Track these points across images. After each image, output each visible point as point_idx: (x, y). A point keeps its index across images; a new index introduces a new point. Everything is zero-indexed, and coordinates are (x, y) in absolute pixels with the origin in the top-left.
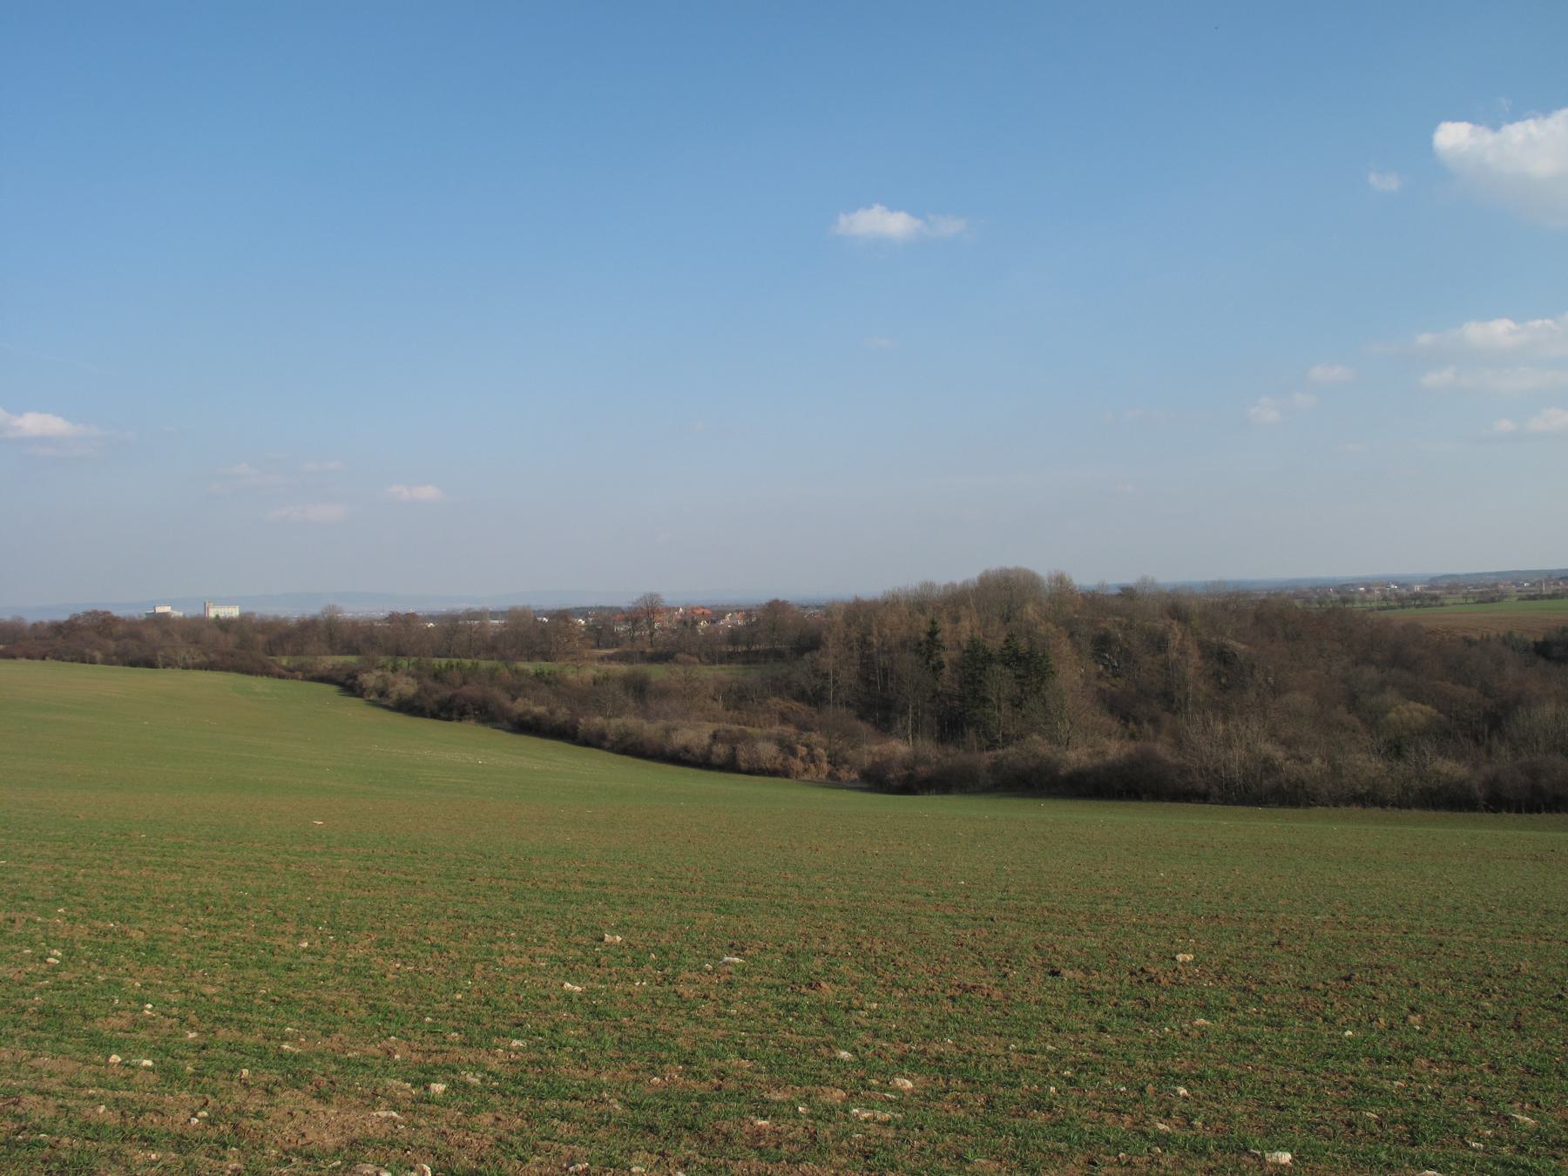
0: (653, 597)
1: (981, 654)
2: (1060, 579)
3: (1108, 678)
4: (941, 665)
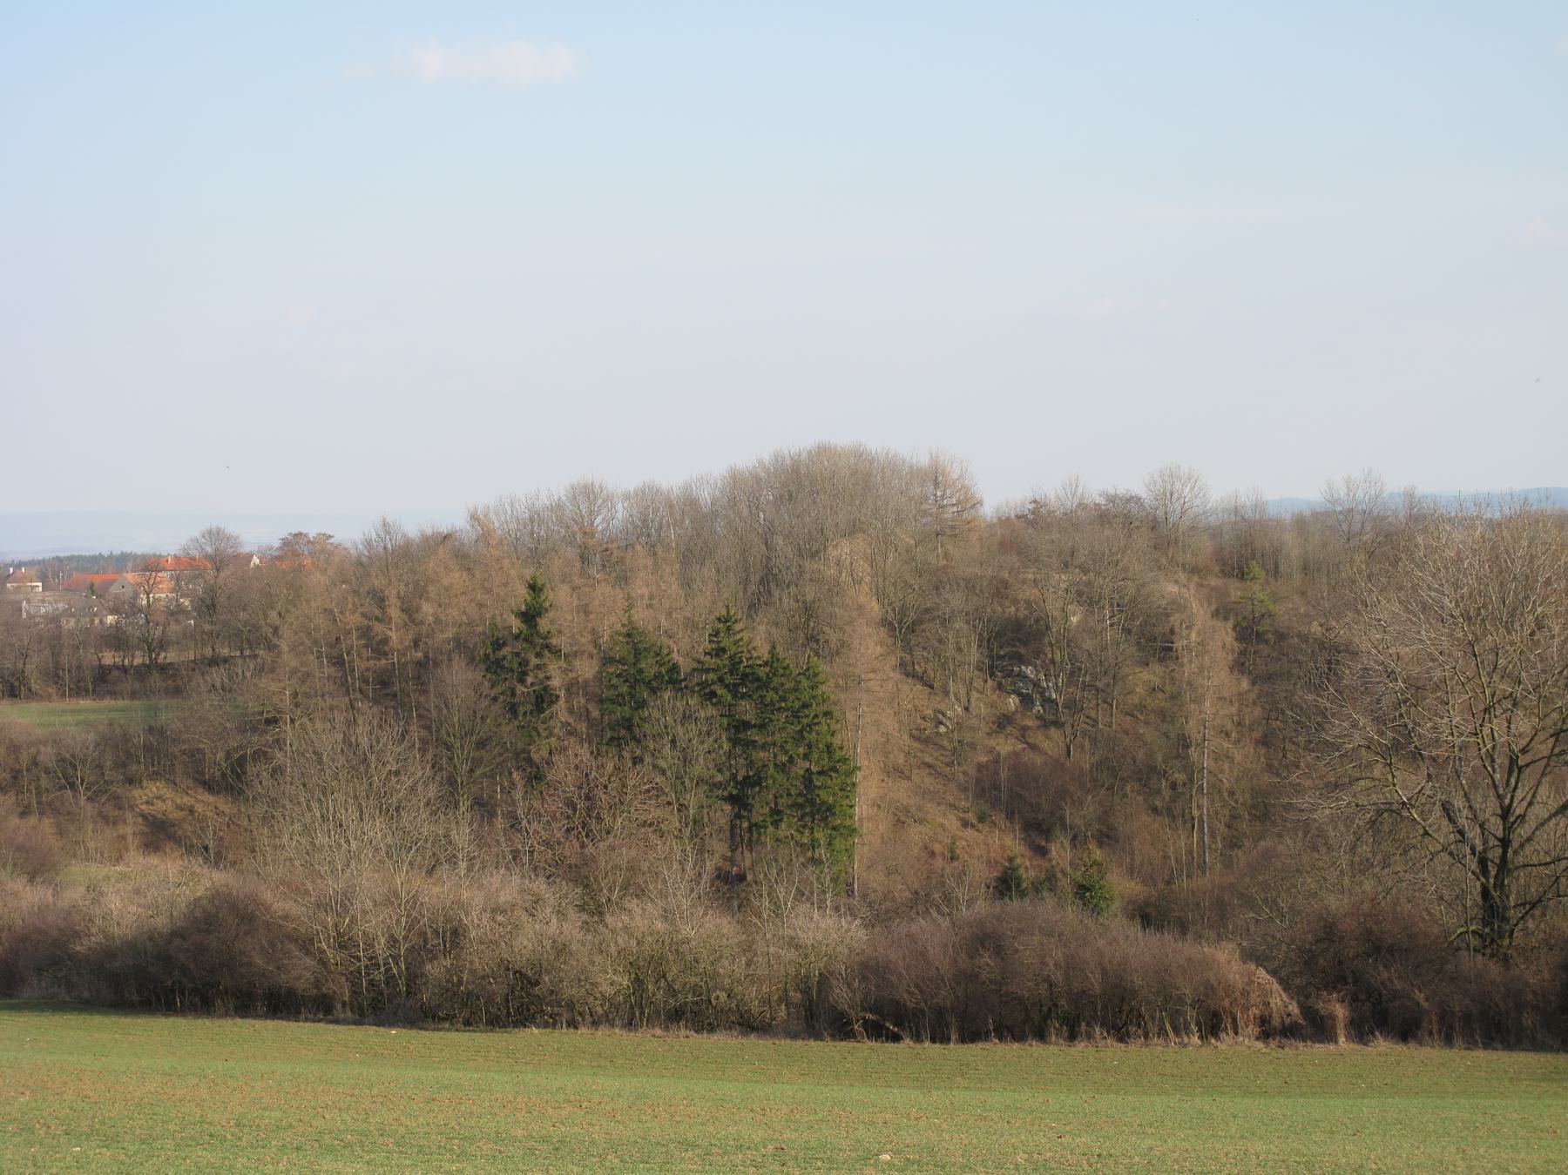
0: (215, 535)
1: (649, 667)
2: (1410, 495)
3: (1025, 729)
4: (543, 699)
